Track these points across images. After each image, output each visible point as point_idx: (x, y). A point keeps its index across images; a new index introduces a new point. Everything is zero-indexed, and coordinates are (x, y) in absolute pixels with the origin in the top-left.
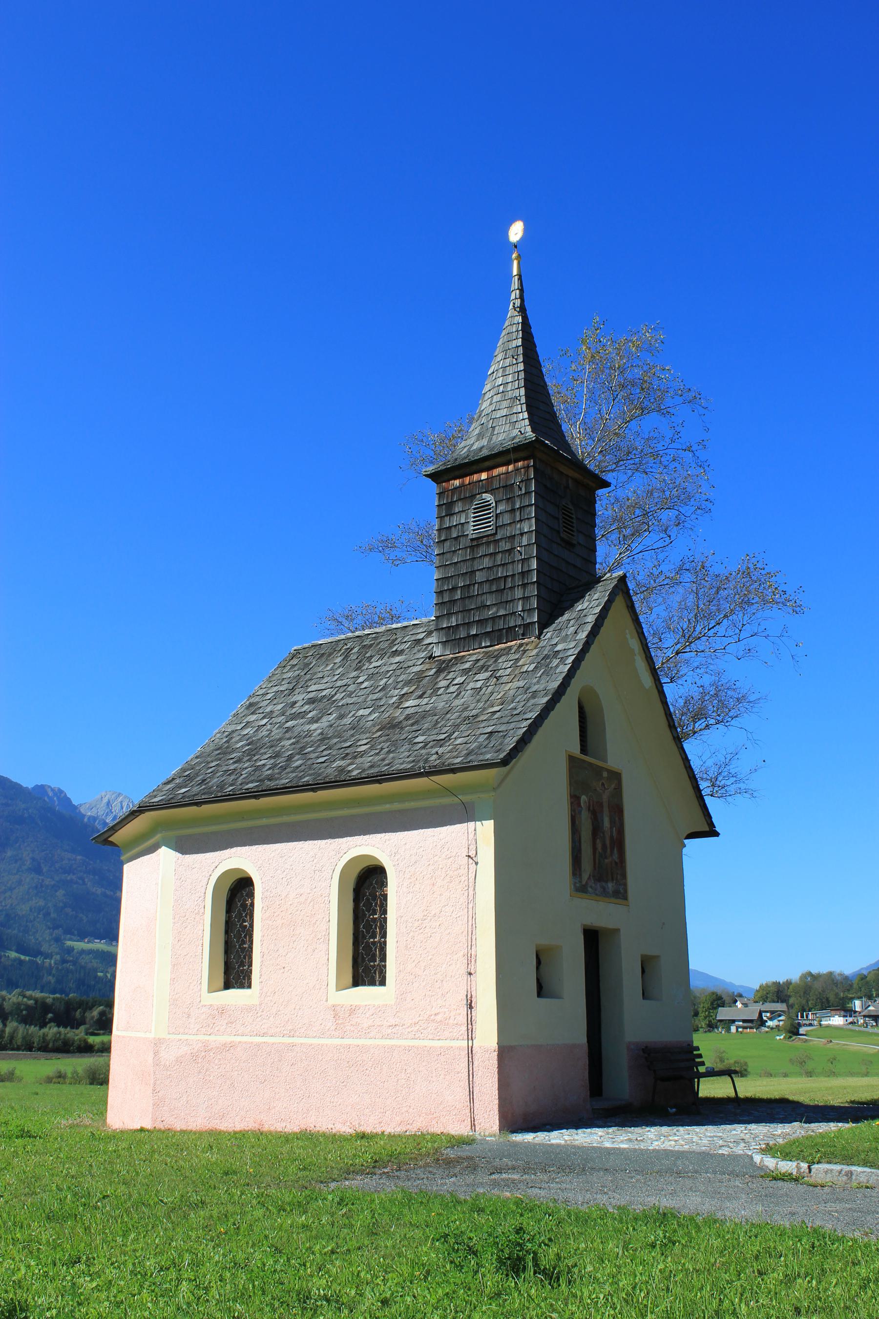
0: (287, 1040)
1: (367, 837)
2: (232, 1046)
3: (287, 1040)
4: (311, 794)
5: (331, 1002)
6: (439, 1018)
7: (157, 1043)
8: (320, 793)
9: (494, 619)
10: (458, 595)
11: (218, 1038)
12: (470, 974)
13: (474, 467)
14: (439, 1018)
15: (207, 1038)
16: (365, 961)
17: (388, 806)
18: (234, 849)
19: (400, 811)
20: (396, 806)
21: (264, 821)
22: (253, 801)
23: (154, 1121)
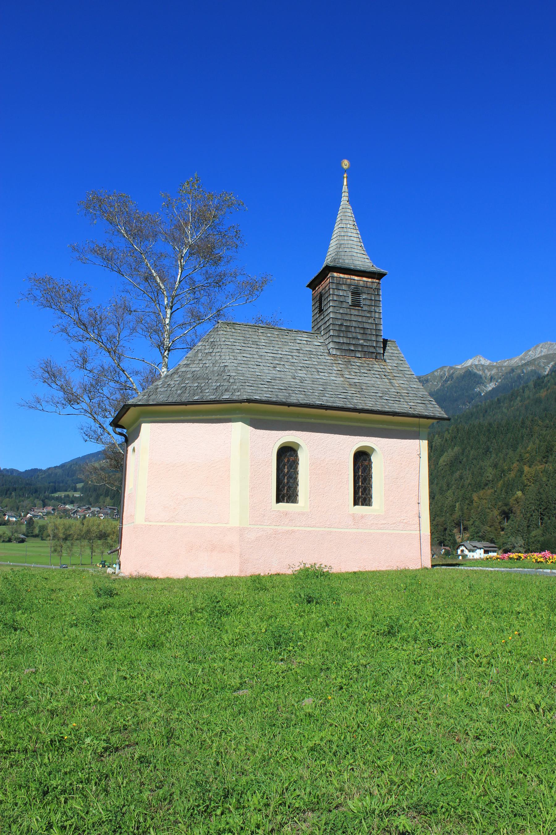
0: (329, 529)
1: (368, 438)
2: (293, 531)
3: (329, 529)
4: (391, 417)
5: (351, 512)
6: (405, 521)
7: (241, 531)
8: (361, 414)
9: (362, 345)
10: (343, 328)
11: (284, 528)
12: (419, 503)
13: (352, 272)
14: (405, 521)
15: (276, 527)
16: (362, 494)
17: (381, 426)
18: (292, 432)
19: (385, 429)
20: (385, 426)
21: (313, 421)
22: (324, 411)
23: (241, 571)
